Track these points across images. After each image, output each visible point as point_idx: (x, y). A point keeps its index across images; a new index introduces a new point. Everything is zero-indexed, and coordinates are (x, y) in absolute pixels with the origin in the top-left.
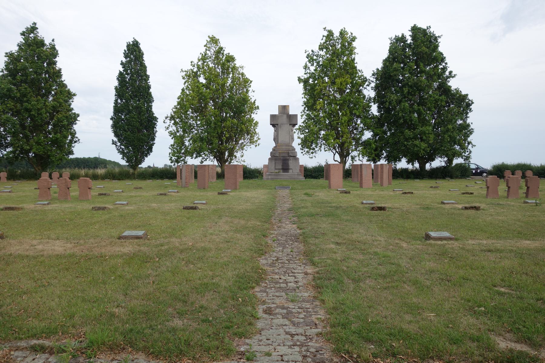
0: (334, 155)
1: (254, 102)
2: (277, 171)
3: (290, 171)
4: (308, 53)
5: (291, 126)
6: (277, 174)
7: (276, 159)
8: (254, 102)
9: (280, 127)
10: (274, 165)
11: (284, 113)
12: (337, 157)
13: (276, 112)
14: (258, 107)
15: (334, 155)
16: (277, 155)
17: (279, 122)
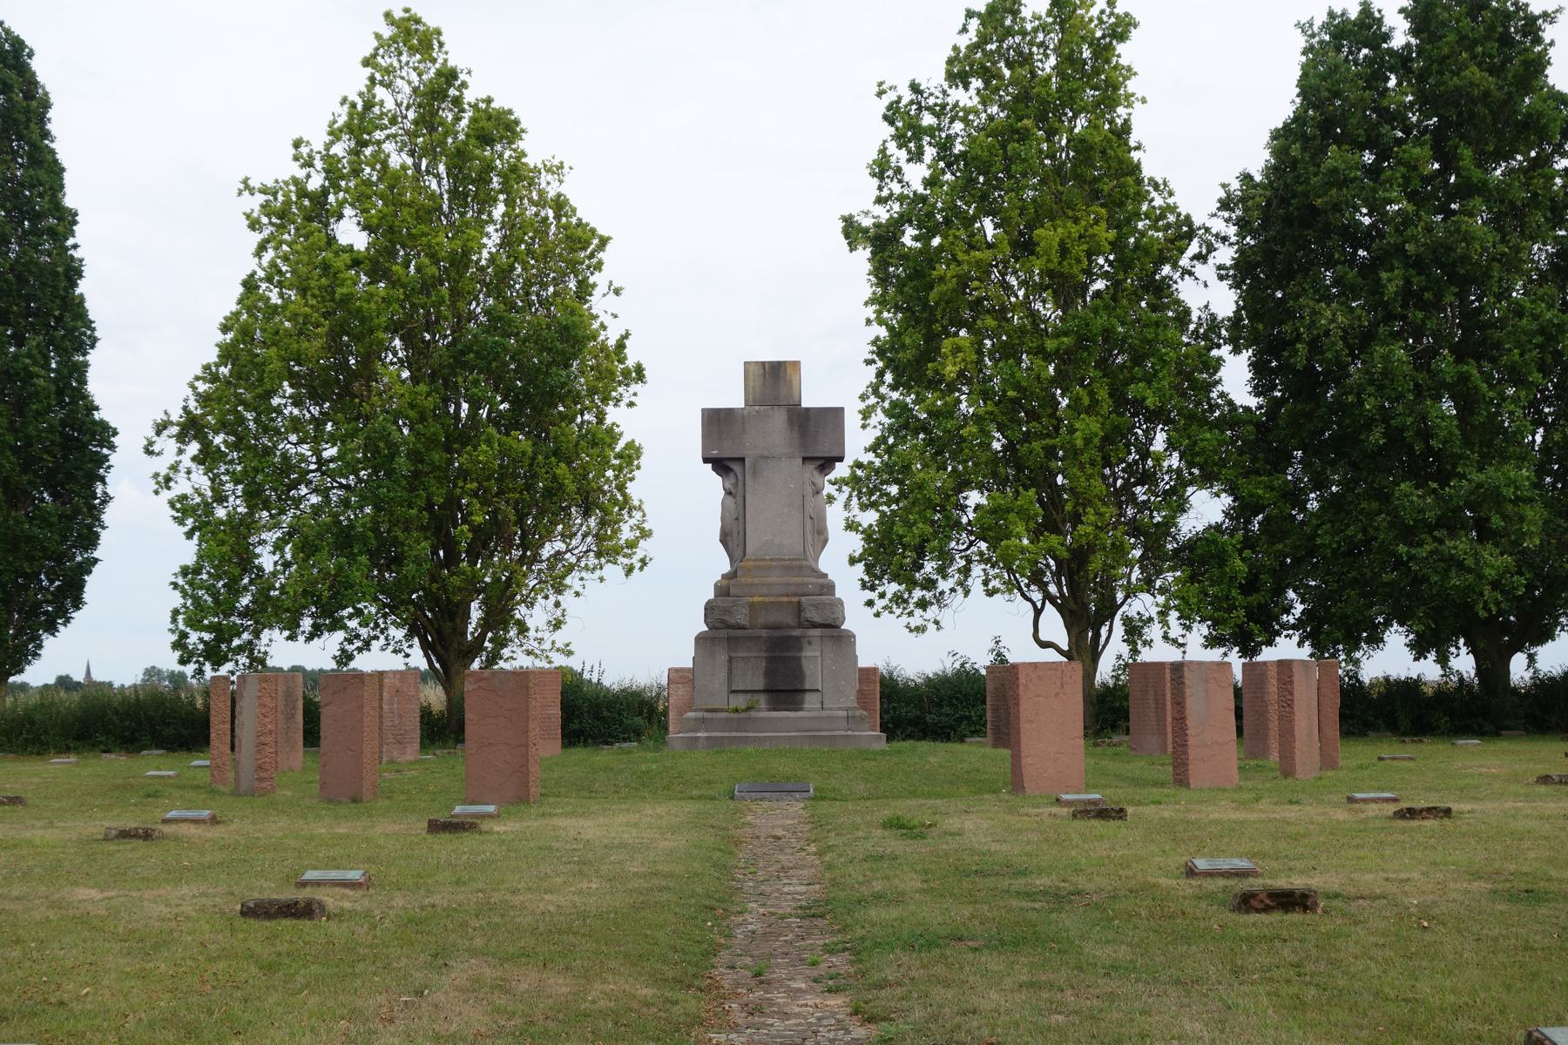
0: (1038, 612)
2: (740, 701)
3: (811, 701)
4: (890, 97)
5: (811, 467)
6: (740, 719)
7: (732, 642)
8: (621, 346)
11: (775, 404)
12: (1054, 626)
13: (733, 397)
14: (639, 370)
15: (1038, 612)
16: (741, 617)
17: (750, 446)
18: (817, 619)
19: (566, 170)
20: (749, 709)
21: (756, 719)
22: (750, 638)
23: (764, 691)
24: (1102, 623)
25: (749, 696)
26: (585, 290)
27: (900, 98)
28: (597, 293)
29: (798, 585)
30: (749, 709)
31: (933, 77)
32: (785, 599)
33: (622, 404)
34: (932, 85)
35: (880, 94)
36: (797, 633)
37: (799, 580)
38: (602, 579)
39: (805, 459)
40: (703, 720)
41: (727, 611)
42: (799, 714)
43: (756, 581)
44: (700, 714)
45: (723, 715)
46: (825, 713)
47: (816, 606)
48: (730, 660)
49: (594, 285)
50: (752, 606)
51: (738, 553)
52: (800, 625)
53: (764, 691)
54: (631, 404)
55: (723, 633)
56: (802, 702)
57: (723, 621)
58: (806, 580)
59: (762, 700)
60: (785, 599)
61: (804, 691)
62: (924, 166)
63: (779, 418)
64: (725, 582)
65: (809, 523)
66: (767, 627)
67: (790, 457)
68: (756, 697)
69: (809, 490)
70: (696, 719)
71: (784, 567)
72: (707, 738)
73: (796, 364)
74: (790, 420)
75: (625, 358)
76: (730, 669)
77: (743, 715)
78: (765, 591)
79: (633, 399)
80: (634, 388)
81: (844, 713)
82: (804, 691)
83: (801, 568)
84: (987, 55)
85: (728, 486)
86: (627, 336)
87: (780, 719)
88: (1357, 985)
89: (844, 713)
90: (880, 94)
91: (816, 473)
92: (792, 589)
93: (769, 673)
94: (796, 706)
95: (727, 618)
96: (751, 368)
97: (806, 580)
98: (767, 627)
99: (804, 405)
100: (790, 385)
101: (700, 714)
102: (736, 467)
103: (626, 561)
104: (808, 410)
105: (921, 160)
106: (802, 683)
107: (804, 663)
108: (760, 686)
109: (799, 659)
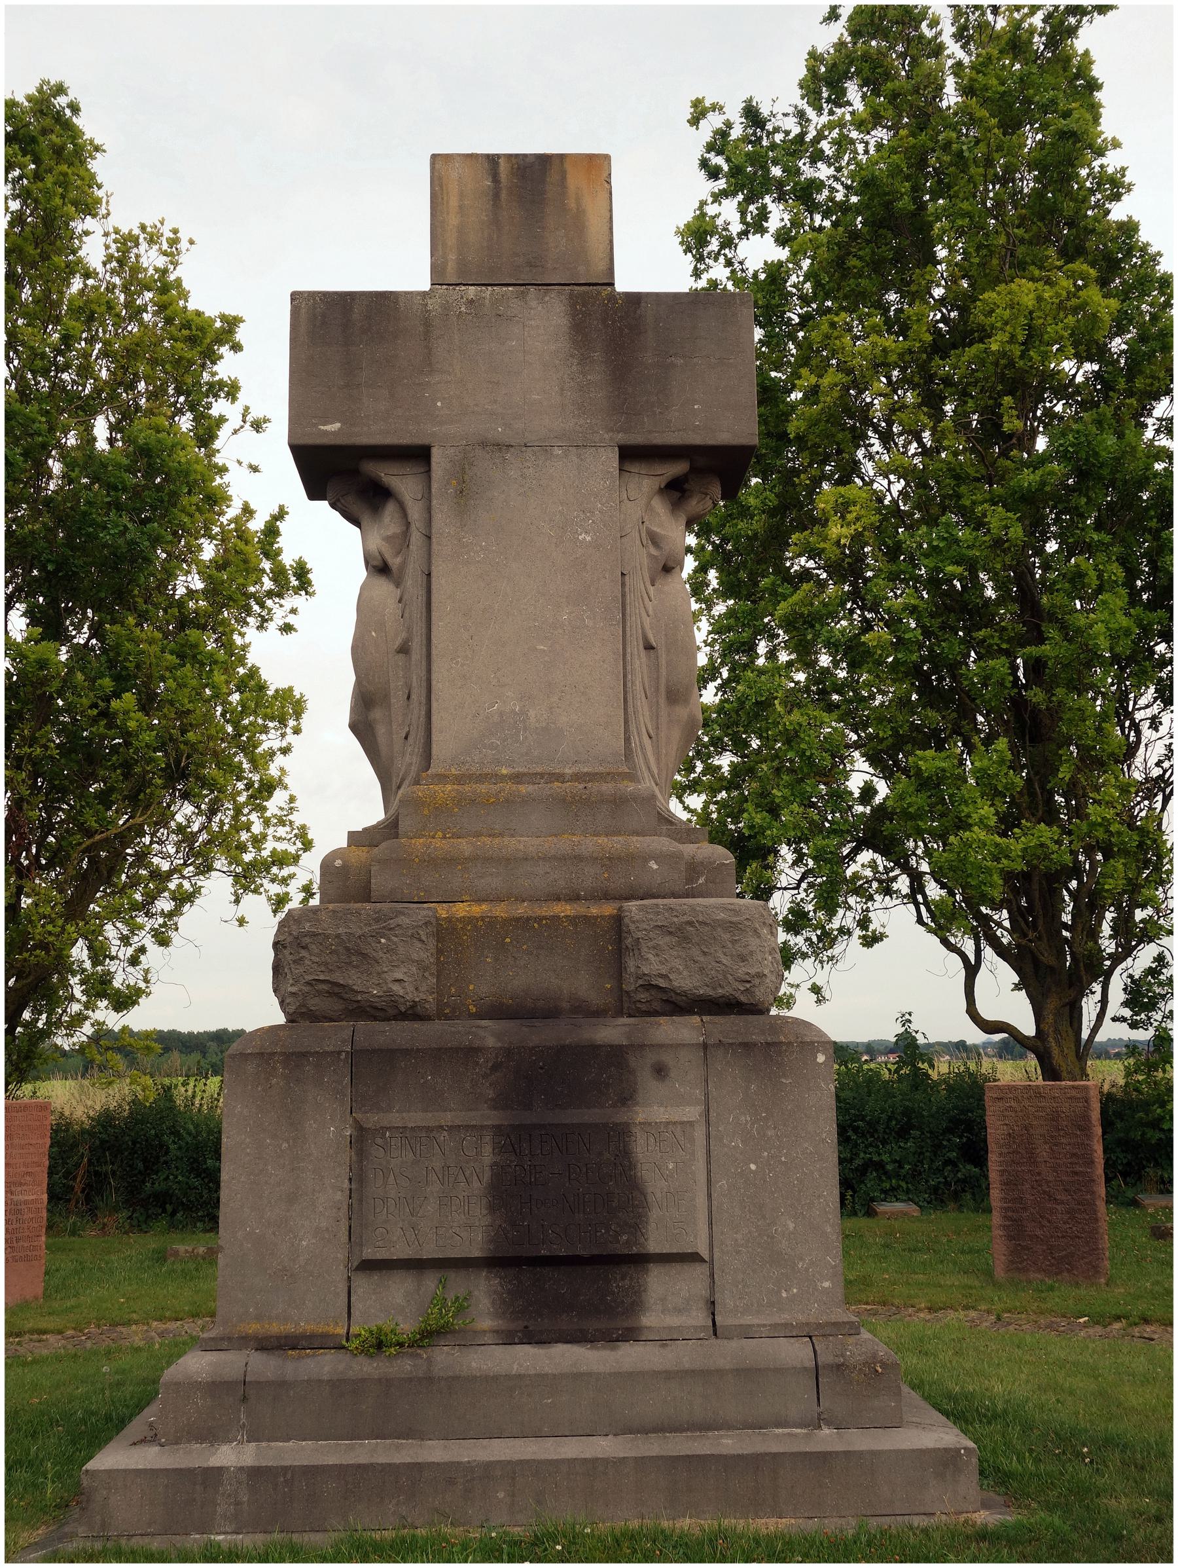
0: (972, 970)
1: (271, 531)
2: (393, 1305)
3: (668, 1299)
4: (714, 121)
5: (646, 483)
6: (394, 1384)
7: (370, 1071)
8: (271, 531)
9: (465, 493)
10: (329, 1194)
11: (531, 282)
12: (1005, 998)
13: (395, 258)
14: (302, 571)
15: (972, 970)
16: (403, 976)
17: (447, 408)
18: (686, 981)
19: (183, 245)
20: (429, 1336)
21: (457, 1382)
22: (439, 1055)
23: (492, 1263)
24: (1082, 991)
25: (431, 1282)
26: (207, 433)
27: (729, 125)
28: (224, 433)
29: (611, 861)
30: (429, 1336)
31: (782, 96)
32: (565, 909)
33: (272, 626)
34: (779, 108)
35: (695, 121)
36: (611, 1032)
37: (616, 844)
38: (242, 922)
39: (630, 455)
40: (241, 1390)
41: (356, 953)
42: (629, 1356)
43: (465, 846)
44: (231, 1363)
45: (325, 1365)
46: (724, 1354)
47: (681, 933)
48: (361, 1139)
49: (222, 420)
50: (445, 934)
51: (407, 760)
52: (623, 1005)
53: (492, 1263)
54: (287, 628)
55: (336, 1036)
56: (635, 1305)
57: (337, 991)
58: (638, 843)
59: (482, 1297)
60: (565, 909)
61: (643, 1260)
62: (768, 239)
63: (544, 323)
64: (361, 854)
65: (640, 661)
66: (497, 1011)
67: (581, 444)
68: (458, 1284)
69: (641, 558)
70: (216, 1388)
71: (564, 802)
72: (255, 1473)
73: (596, 166)
74: (579, 329)
75: (279, 552)
76: (358, 1179)
77: (405, 1366)
78: (493, 881)
79: (291, 619)
80: (290, 601)
81: (797, 1353)
82: (643, 1260)
83: (619, 802)
84: (874, 57)
85: (376, 543)
86: (281, 514)
87: (549, 1382)
88: (1033, 1317)
89: (797, 1353)
90: (695, 121)
91: (660, 506)
92: (590, 876)
93: (508, 1193)
94: (612, 1322)
95: (353, 979)
96: (453, 174)
97: (638, 843)
98: (497, 1011)
99: (624, 283)
100: (578, 224)
101: (231, 1363)
102: (403, 482)
103: (275, 889)
104: (635, 299)
105: (762, 231)
106: (636, 1226)
107: (643, 1149)
108: (474, 1244)
109: (620, 1135)
